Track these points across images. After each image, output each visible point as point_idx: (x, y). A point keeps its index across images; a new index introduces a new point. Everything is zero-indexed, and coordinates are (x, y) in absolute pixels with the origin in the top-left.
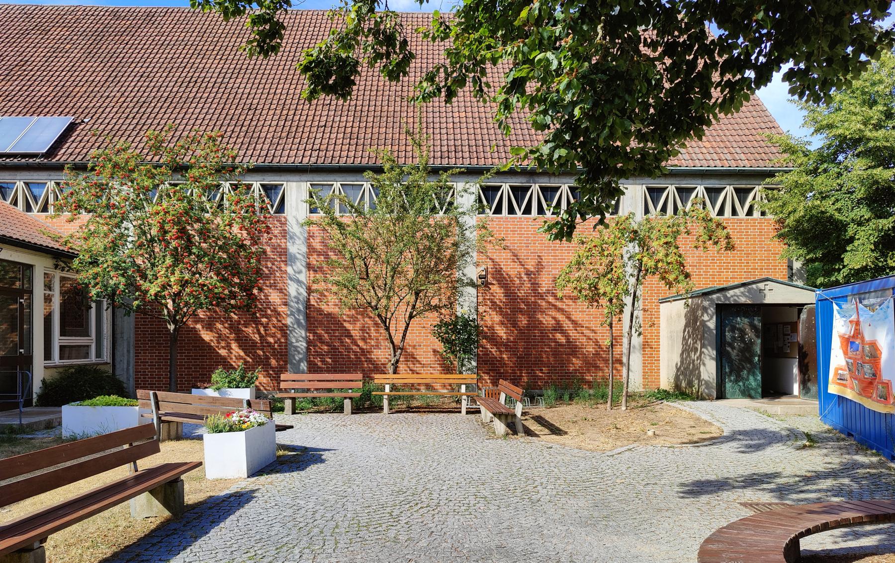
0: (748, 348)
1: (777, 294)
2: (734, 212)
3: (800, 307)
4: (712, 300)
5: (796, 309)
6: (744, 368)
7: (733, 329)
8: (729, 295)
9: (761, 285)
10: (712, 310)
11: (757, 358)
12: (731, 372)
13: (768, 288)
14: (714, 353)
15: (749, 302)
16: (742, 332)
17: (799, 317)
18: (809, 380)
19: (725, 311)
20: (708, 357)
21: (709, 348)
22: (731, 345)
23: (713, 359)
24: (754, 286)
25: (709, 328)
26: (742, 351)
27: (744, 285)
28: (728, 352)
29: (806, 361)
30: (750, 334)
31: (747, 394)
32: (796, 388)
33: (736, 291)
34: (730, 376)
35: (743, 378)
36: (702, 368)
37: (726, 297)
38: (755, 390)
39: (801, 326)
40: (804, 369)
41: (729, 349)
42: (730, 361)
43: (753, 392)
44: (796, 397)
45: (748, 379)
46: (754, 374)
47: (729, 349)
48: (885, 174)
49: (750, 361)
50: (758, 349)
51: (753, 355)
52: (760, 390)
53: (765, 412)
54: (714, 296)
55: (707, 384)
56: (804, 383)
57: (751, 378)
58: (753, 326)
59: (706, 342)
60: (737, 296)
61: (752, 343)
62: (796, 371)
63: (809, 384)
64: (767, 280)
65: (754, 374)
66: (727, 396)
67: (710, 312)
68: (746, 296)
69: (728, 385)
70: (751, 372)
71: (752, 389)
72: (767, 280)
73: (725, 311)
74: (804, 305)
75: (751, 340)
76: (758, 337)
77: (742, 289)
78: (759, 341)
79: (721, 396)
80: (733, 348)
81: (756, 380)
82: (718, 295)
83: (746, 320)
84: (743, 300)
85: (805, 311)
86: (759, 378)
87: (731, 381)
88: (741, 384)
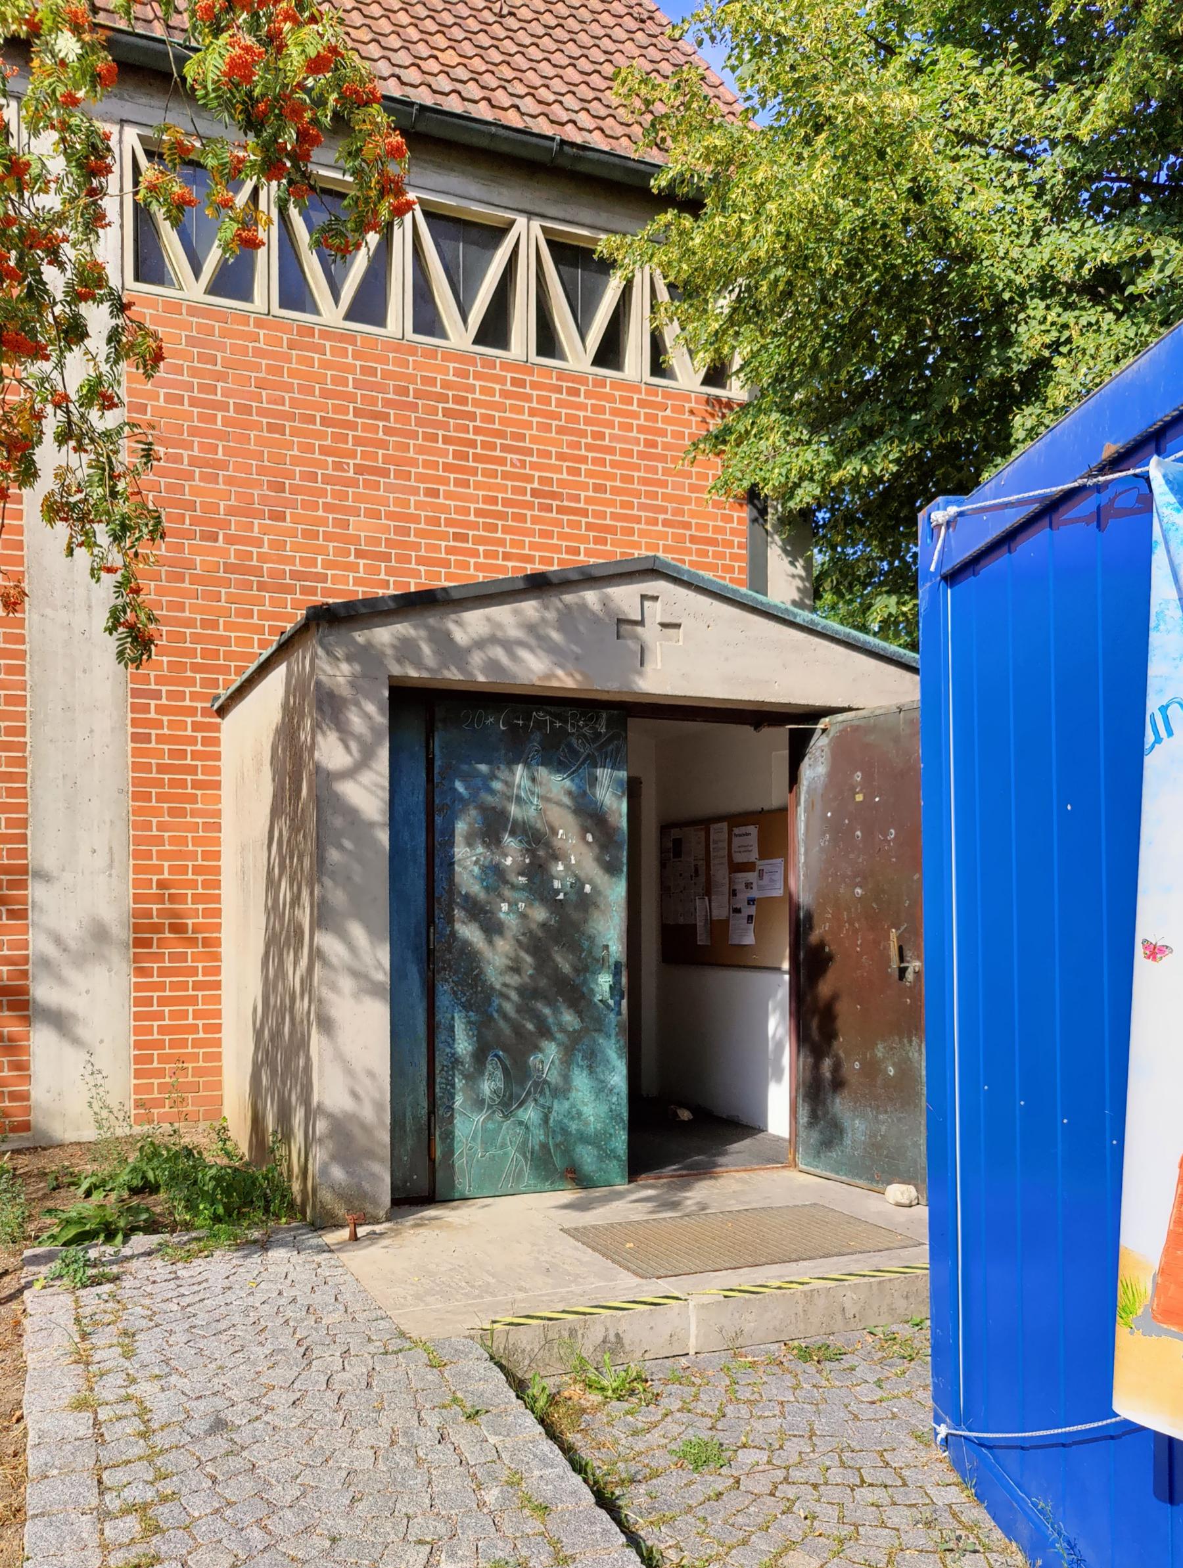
0: (568, 920)
1: (698, 653)
2: (427, 320)
3: (798, 724)
4: (367, 656)
5: (781, 735)
6: (544, 1031)
7: (493, 827)
8: (460, 637)
9: (624, 597)
10: (369, 715)
11: (604, 981)
12: (480, 1055)
13: (656, 612)
14: (378, 958)
15: (566, 681)
16: (538, 843)
17: (794, 779)
18: (838, 1084)
19: (437, 723)
20: (347, 984)
21: (357, 932)
22: (481, 913)
23: (373, 990)
24: (591, 597)
25: (351, 814)
26: (537, 944)
27: (538, 585)
28: (469, 956)
29: (825, 988)
30: (576, 858)
31: (559, 1165)
32: (778, 1107)
33: (502, 613)
34: (472, 1079)
35: (541, 1085)
36: (316, 1040)
37: (443, 643)
38: (598, 1141)
39: (801, 823)
40: (815, 1025)
41: (469, 932)
42: (478, 997)
43: (587, 1156)
44: (775, 1157)
45: (562, 1091)
46: (593, 1060)
47: (469, 932)
48: (12, 1029)
49: (574, 993)
50: (610, 931)
51: (587, 965)
52: (620, 1141)
53: (259, 771)
54: (384, 635)
55: (343, 1132)
56: (815, 1093)
57: (581, 1081)
58: (591, 817)
59: (338, 898)
60: (508, 645)
61: (585, 903)
62: (777, 1025)
63: (840, 1105)
64: (652, 571)
65: (593, 1060)
66: (463, 1184)
67: (356, 721)
68: (552, 650)
69: (468, 1126)
70: (580, 1049)
71: (583, 1138)
72: (652, 571)
73: (437, 723)
74: (815, 714)
75: (579, 884)
76: (610, 869)
77: (530, 608)
78: (616, 891)
79: (422, 1186)
80: (492, 928)
81: (601, 1089)
82: (403, 629)
83: (557, 784)
84: (535, 669)
85: (820, 744)
86: (618, 1078)
87: (479, 1103)
88: (530, 1113)
